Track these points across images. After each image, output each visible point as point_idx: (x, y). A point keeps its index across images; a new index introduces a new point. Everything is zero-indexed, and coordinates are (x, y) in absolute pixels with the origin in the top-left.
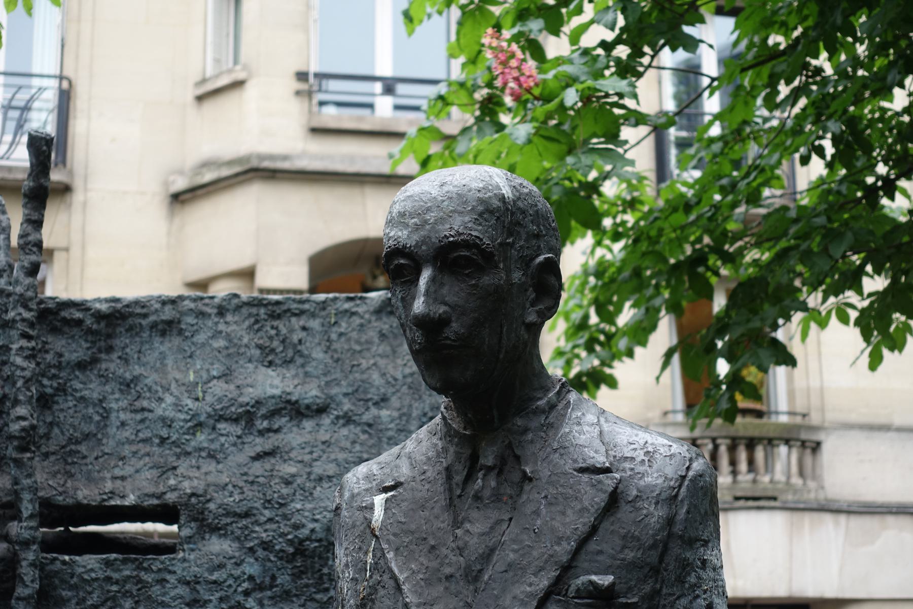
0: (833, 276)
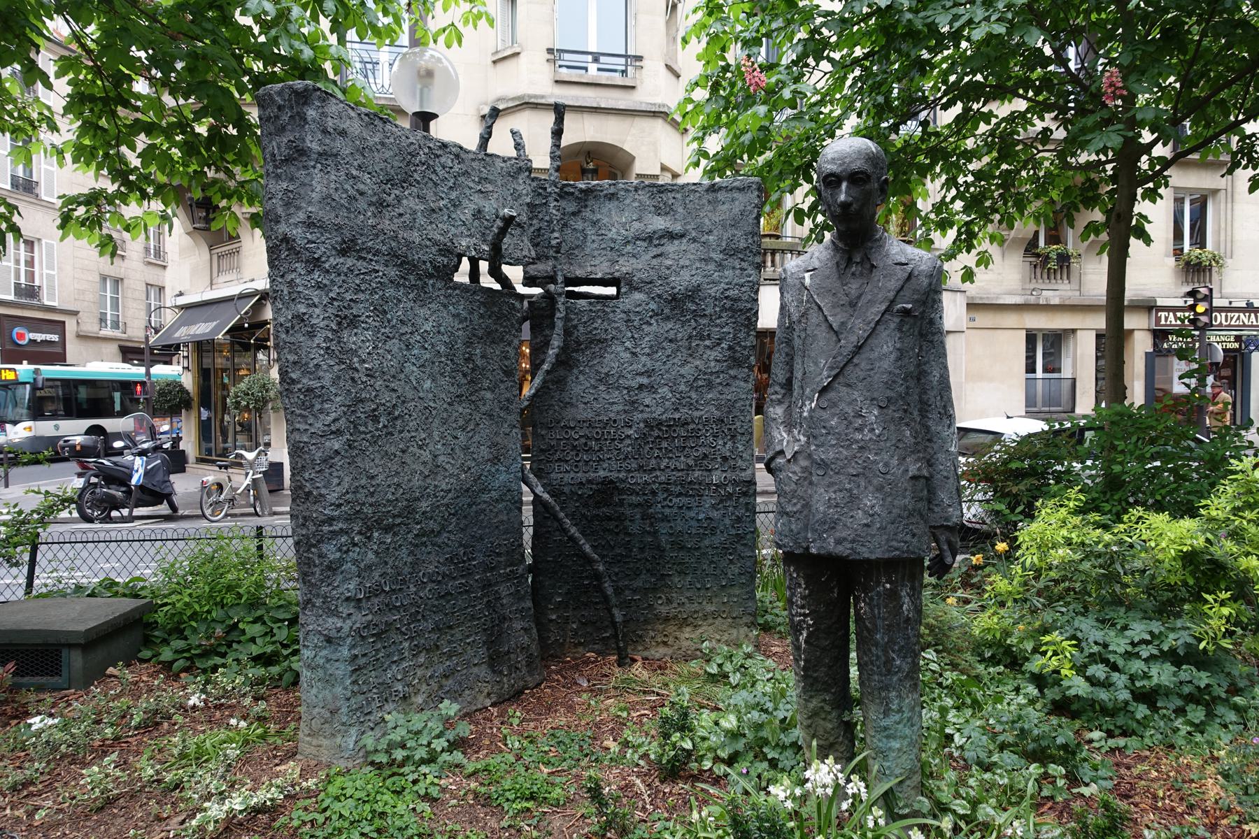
0: (132, 62)
